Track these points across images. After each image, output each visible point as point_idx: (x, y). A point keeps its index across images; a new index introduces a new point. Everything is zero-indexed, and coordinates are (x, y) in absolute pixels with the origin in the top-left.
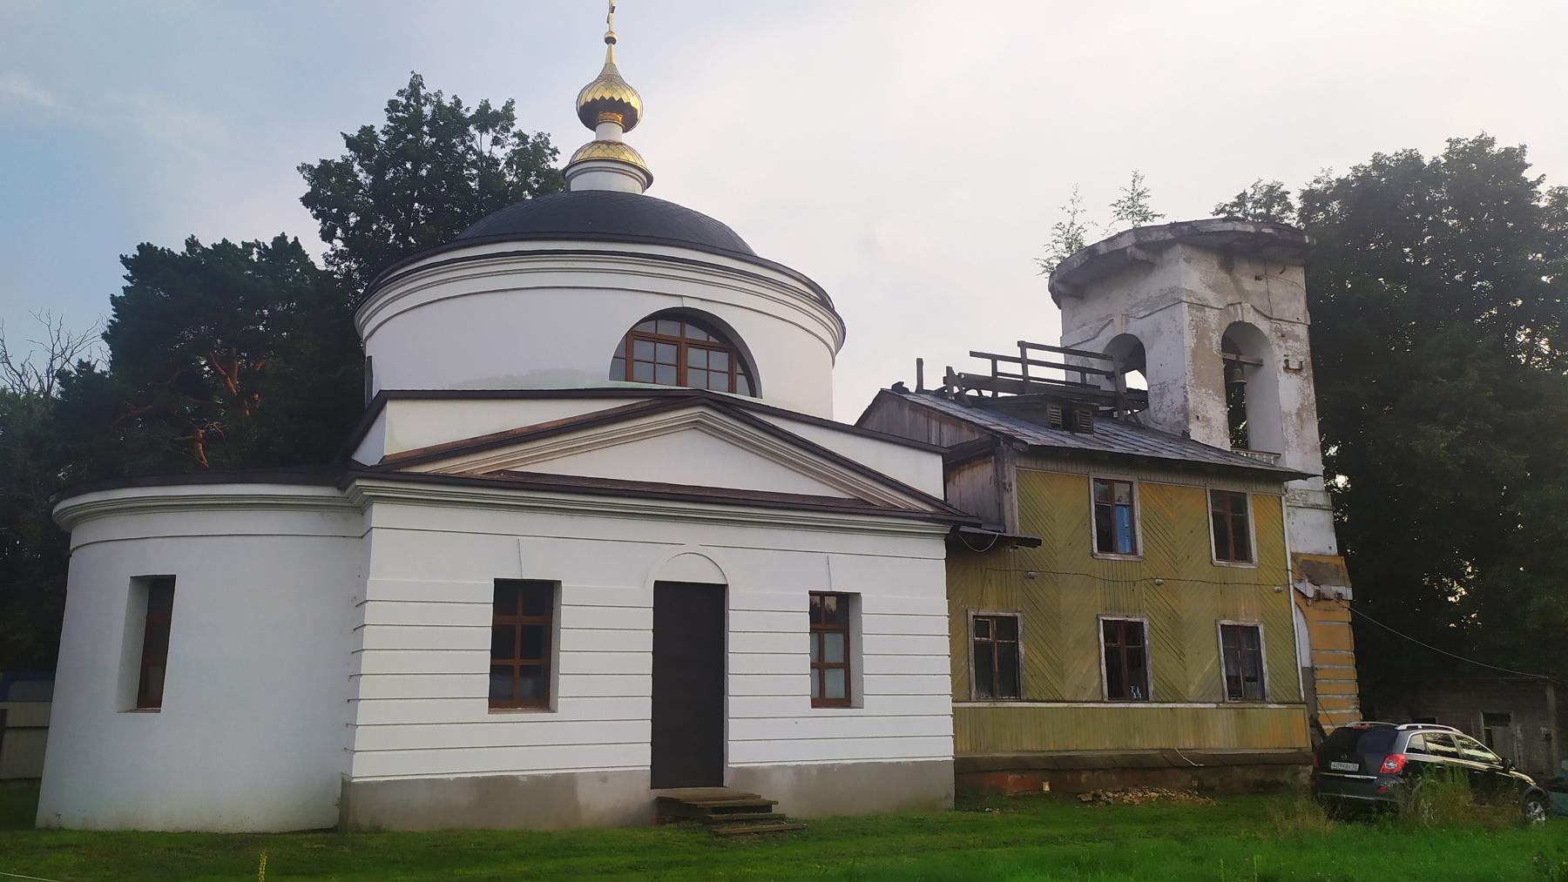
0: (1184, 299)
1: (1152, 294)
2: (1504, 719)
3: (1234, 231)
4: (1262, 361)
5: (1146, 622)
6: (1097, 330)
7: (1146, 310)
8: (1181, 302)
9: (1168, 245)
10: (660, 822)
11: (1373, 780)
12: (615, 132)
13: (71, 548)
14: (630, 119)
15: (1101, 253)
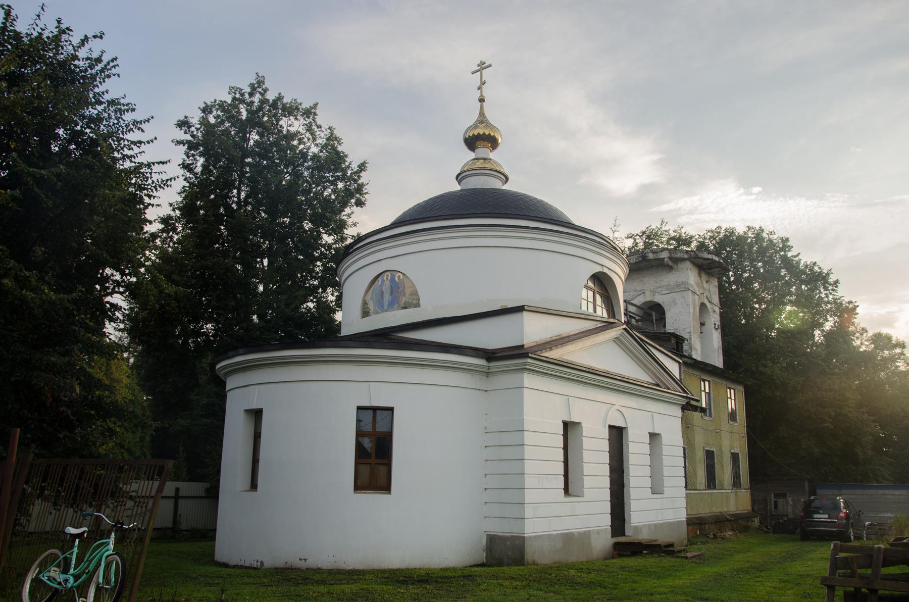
0: (691, 289)
1: (671, 283)
2: (784, 496)
3: (712, 259)
4: (705, 322)
5: (715, 451)
6: (634, 296)
7: (667, 290)
8: (689, 290)
9: (683, 260)
10: (620, 555)
11: (836, 522)
12: (482, 152)
13: (227, 390)
14: (493, 142)
15: (650, 258)
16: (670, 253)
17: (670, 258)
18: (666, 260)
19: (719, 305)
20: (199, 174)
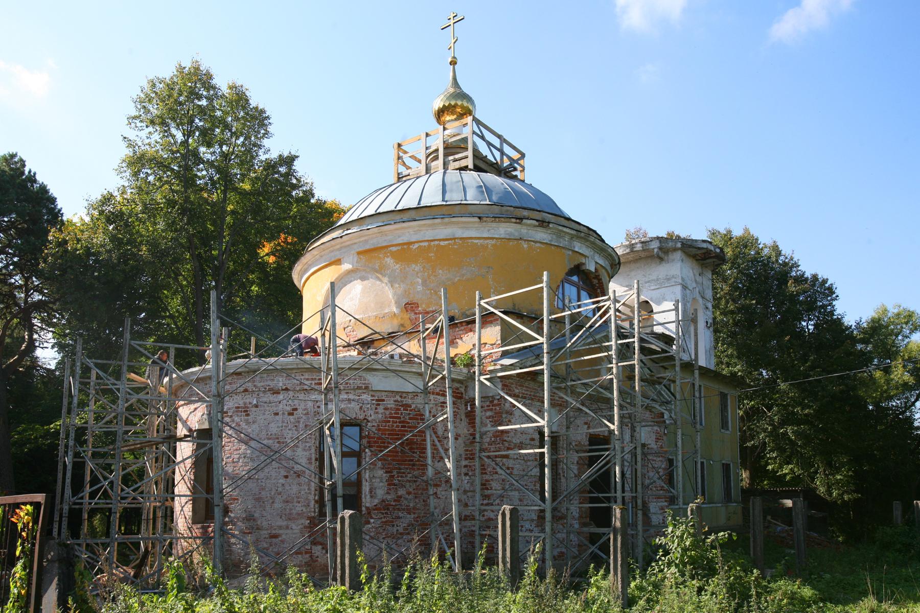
9: (675, 250)
16: (660, 242)
17: (660, 248)
18: (656, 250)
19: (712, 300)
20: (267, 156)
